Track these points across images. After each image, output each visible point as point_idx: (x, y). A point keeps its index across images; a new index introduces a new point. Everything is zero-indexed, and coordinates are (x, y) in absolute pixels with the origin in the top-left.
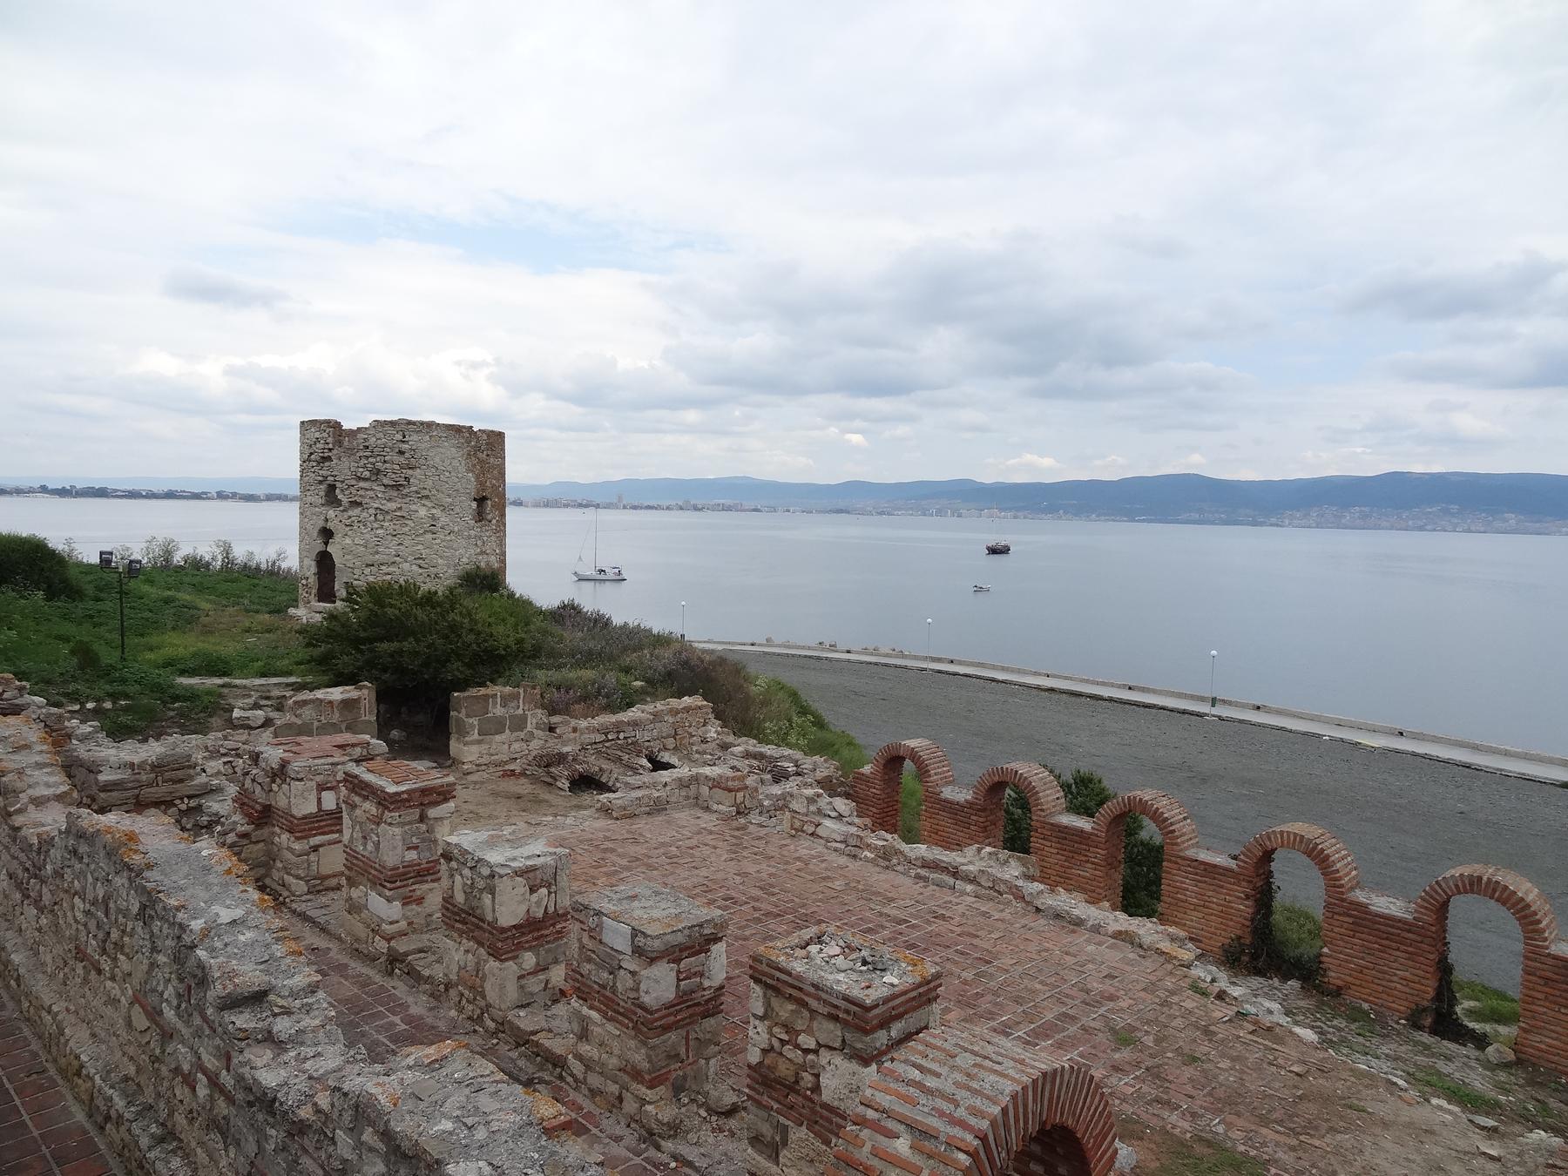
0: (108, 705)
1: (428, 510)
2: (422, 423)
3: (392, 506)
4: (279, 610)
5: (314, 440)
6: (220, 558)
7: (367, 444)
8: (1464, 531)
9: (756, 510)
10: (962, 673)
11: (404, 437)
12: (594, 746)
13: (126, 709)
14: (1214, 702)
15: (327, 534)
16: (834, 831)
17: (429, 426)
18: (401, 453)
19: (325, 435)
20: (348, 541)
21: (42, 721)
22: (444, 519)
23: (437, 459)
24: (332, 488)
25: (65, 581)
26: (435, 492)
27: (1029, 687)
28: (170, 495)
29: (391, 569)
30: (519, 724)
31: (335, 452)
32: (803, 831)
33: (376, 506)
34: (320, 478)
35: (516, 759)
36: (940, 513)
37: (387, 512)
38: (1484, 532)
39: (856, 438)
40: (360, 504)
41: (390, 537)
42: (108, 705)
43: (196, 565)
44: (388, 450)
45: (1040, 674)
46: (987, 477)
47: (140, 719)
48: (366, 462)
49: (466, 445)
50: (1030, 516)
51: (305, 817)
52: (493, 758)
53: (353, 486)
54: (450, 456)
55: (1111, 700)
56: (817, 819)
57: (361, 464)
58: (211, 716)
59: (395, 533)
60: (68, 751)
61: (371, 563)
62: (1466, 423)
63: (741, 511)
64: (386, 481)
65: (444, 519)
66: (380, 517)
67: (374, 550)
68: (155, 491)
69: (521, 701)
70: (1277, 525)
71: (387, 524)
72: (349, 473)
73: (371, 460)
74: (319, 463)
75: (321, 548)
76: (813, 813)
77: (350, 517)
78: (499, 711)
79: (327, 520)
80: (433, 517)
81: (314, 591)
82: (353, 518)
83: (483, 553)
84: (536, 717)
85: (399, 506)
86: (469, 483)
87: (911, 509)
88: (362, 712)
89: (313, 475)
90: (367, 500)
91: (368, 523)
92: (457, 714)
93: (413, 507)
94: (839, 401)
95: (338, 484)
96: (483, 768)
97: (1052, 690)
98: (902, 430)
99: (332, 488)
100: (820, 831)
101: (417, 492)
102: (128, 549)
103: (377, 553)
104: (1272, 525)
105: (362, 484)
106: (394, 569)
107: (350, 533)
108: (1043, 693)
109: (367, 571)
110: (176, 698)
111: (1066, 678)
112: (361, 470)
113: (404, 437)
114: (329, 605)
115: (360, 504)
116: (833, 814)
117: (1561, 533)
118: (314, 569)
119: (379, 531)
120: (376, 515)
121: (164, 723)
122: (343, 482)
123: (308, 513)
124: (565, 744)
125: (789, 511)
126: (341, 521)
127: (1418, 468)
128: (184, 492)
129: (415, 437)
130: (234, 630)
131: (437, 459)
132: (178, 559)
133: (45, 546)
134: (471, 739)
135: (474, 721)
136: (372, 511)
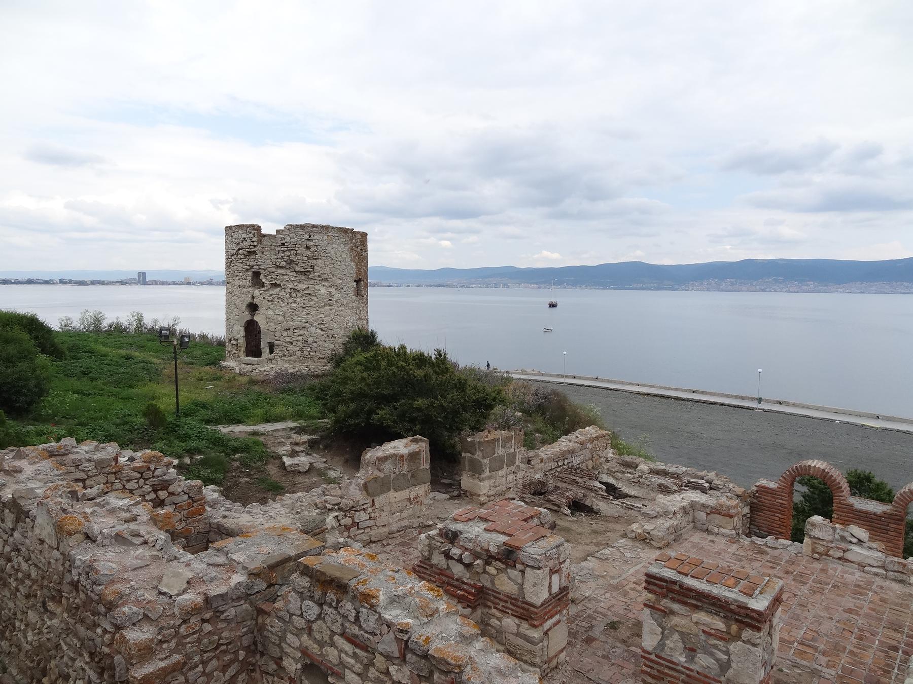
0: (187, 460)
1: (326, 289)
2: (322, 227)
3: (301, 286)
4: (214, 363)
5: (242, 239)
6: (135, 323)
7: (283, 242)
8: (786, 292)
9: (390, 286)
10: (586, 384)
11: (310, 236)
12: (551, 472)
13: (203, 463)
14: (760, 400)
15: (253, 307)
16: (868, 557)
17: (327, 228)
18: (308, 248)
19: (251, 235)
20: (270, 312)
21: (185, 493)
22: (337, 296)
23: (332, 253)
24: (256, 275)
25: (53, 345)
26: (331, 276)
27: (632, 393)
28: (30, 282)
29: (302, 332)
30: (512, 462)
31: (258, 248)
32: (828, 555)
33: (291, 286)
34: (248, 267)
35: (510, 488)
36: (496, 286)
37: (298, 291)
38: (798, 292)
39: (446, 243)
40: (279, 285)
41: (301, 309)
42: (187, 460)
43: (118, 330)
44: (299, 246)
45: (633, 384)
46: (522, 265)
47: (216, 472)
48: (283, 255)
49: (350, 242)
50: (548, 287)
51: (543, 604)
52: (497, 489)
53: (273, 272)
54: (339, 250)
55: (688, 400)
56: (843, 545)
57: (280, 256)
58: (266, 464)
59: (305, 306)
60: (207, 518)
61: (288, 328)
62: (786, 231)
63: (381, 286)
64: (297, 269)
65: (337, 296)
66: (293, 295)
67: (290, 318)
68: (20, 279)
69: (513, 441)
70: (686, 290)
71: (298, 300)
72: (271, 264)
73: (287, 253)
74: (246, 256)
75: (249, 318)
76: (837, 540)
77: (271, 295)
78: (500, 451)
79: (253, 297)
80: (330, 294)
81: (243, 349)
82: (274, 296)
83: (360, 319)
84: (522, 453)
85: (307, 286)
86: (351, 269)
87: (480, 284)
88: (422, 462)
89: (241, 265)
90: (284, 283)
91: (285, 300)
92: (470, 455)
93: (317, 287)
94: (436, 221)
95: (262, 272)
96: (492, 498)
97: (648, 394)
98: (472, 238)
99: (256, 275)
100: (848, 556)
101: (319, 276)
102: (69, 319)
103: (292, 320)
104: (683, 290)
105: (279, 271)
106: (305, 332)
107: (272, 306)
108: (640, 396)
109: (285, 334)
110: (236, 450)
111: (651, 386)
112: (279, 260)
113: (310, 236)
114: (256, 359)
115: (279, 285)
116: (855, 540)
117: (838, 292)
118: (242, 333)
119: (293, 305)
120: (290, 293)
121: (234, 474)
122: (265, 270)
123: (237, 292)
124: (536, 472)
125: (409, 286)
126: (264, 298)
127: (760, 257)
128: (38, 280)
129: (318, 237)
130: (189, 379)
131: (332, 253)
132: (105, 325)
133: (37, 320)
134: (485, 475)
135: (486, 461)
136: (288, 290)
